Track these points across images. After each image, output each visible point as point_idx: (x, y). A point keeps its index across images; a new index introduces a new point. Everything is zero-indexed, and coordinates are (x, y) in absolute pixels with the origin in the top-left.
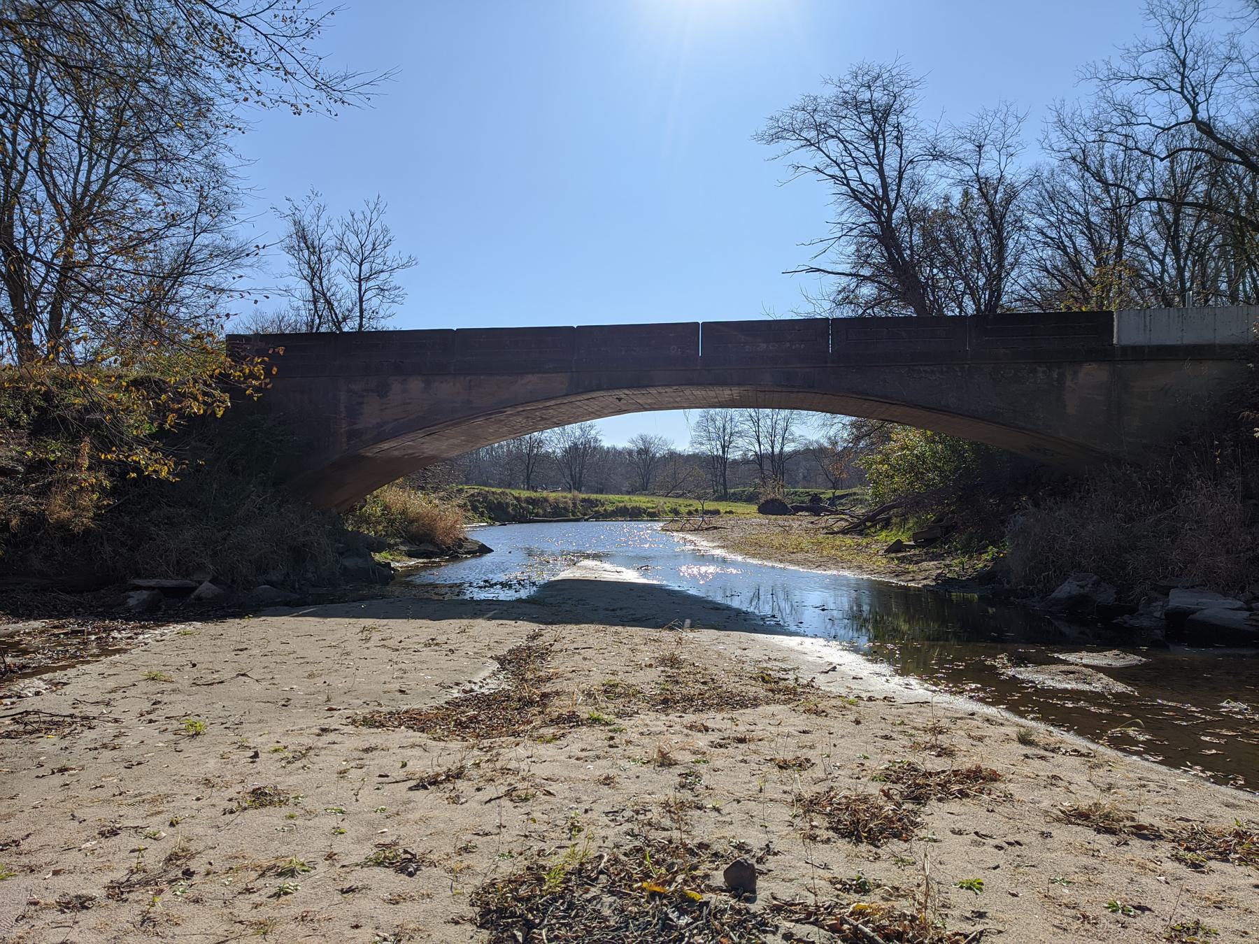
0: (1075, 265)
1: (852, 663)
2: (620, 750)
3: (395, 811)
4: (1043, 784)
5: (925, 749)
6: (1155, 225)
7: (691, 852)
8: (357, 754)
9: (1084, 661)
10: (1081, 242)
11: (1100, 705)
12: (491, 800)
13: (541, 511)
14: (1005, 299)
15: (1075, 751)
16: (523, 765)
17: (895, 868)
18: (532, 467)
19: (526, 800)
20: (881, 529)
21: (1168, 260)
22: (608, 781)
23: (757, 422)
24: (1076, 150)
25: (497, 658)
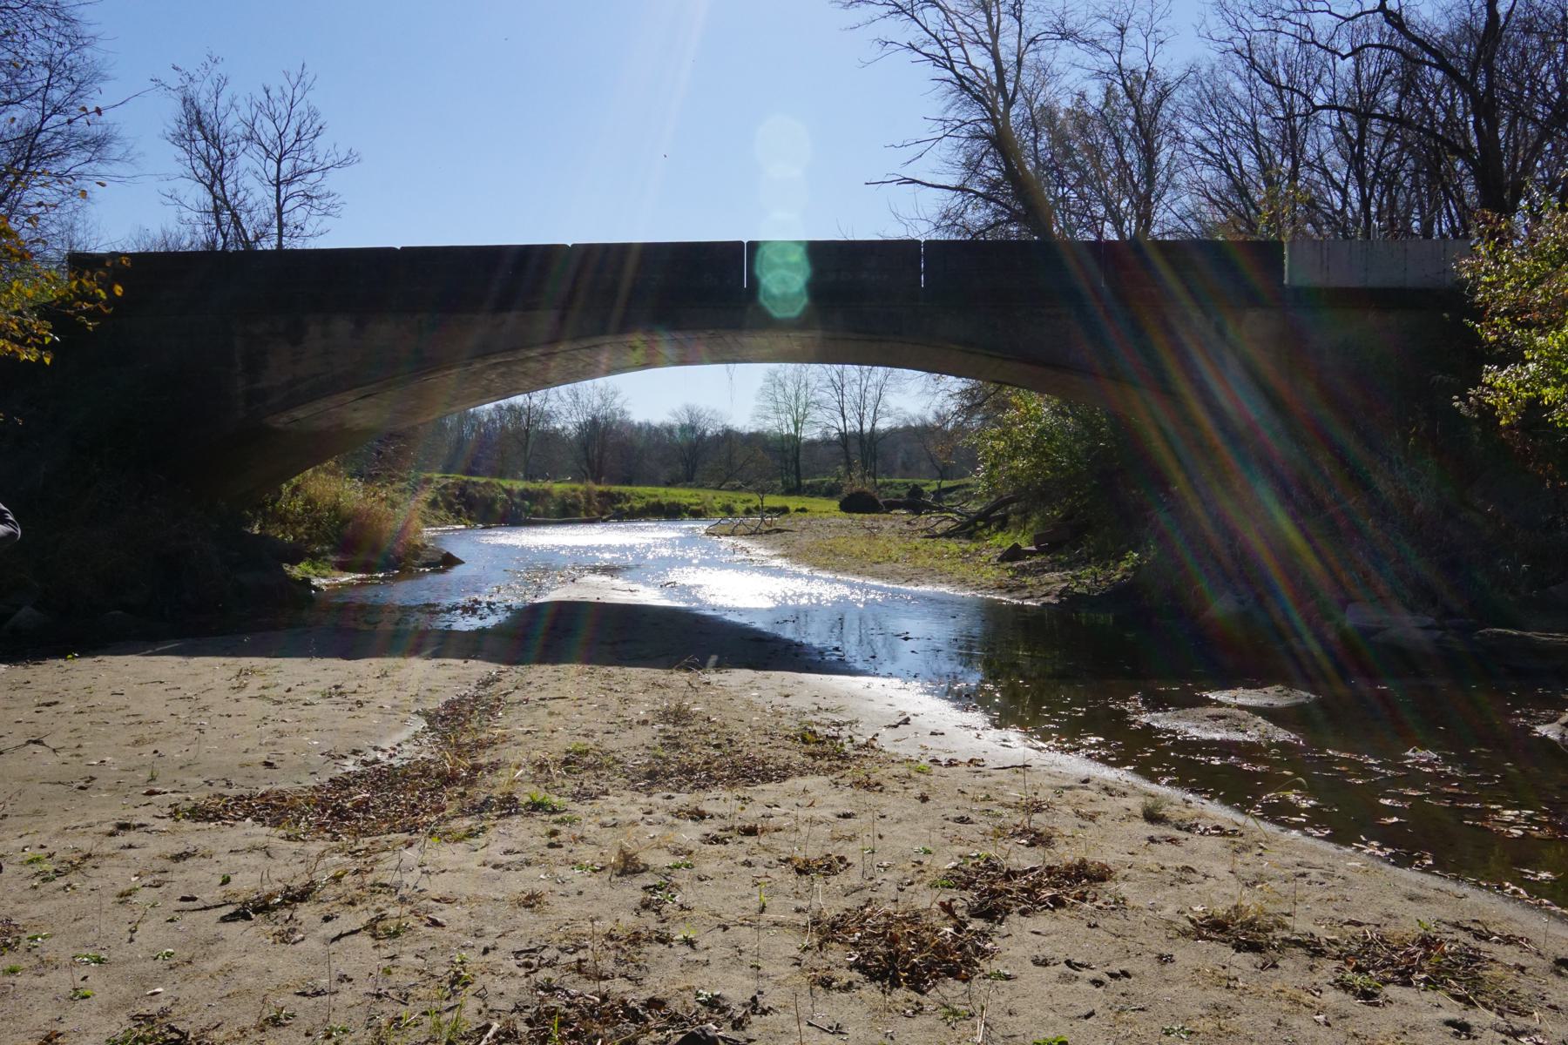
0: (1241, 190)
1: (935, 711)
2: (563, 852)
3: (187, 955)
4: (1169, 879)
5: (1013, 835)
6: (1336, 142)
7: (633, 1015)
8: (159, 864)
9: (1240, 701)
10: (1249, 161)
11: (1255, 761)
12: (341, 936)
13: (541, 509)
14: (1156, 230)
15: (1217, 828)
16: (409, 879)
17: (942, 1025)
18: (531, 446)
19: (396, 934)
20: (997, 531)
21: (1350, 188)
22: (531, 901)
23: (840, 390)
24: (1240, 43)
25: (425, 714)
